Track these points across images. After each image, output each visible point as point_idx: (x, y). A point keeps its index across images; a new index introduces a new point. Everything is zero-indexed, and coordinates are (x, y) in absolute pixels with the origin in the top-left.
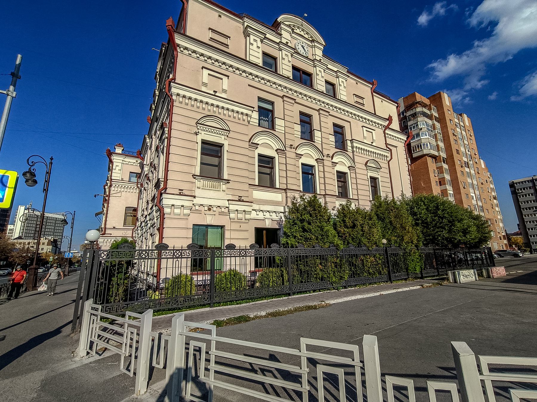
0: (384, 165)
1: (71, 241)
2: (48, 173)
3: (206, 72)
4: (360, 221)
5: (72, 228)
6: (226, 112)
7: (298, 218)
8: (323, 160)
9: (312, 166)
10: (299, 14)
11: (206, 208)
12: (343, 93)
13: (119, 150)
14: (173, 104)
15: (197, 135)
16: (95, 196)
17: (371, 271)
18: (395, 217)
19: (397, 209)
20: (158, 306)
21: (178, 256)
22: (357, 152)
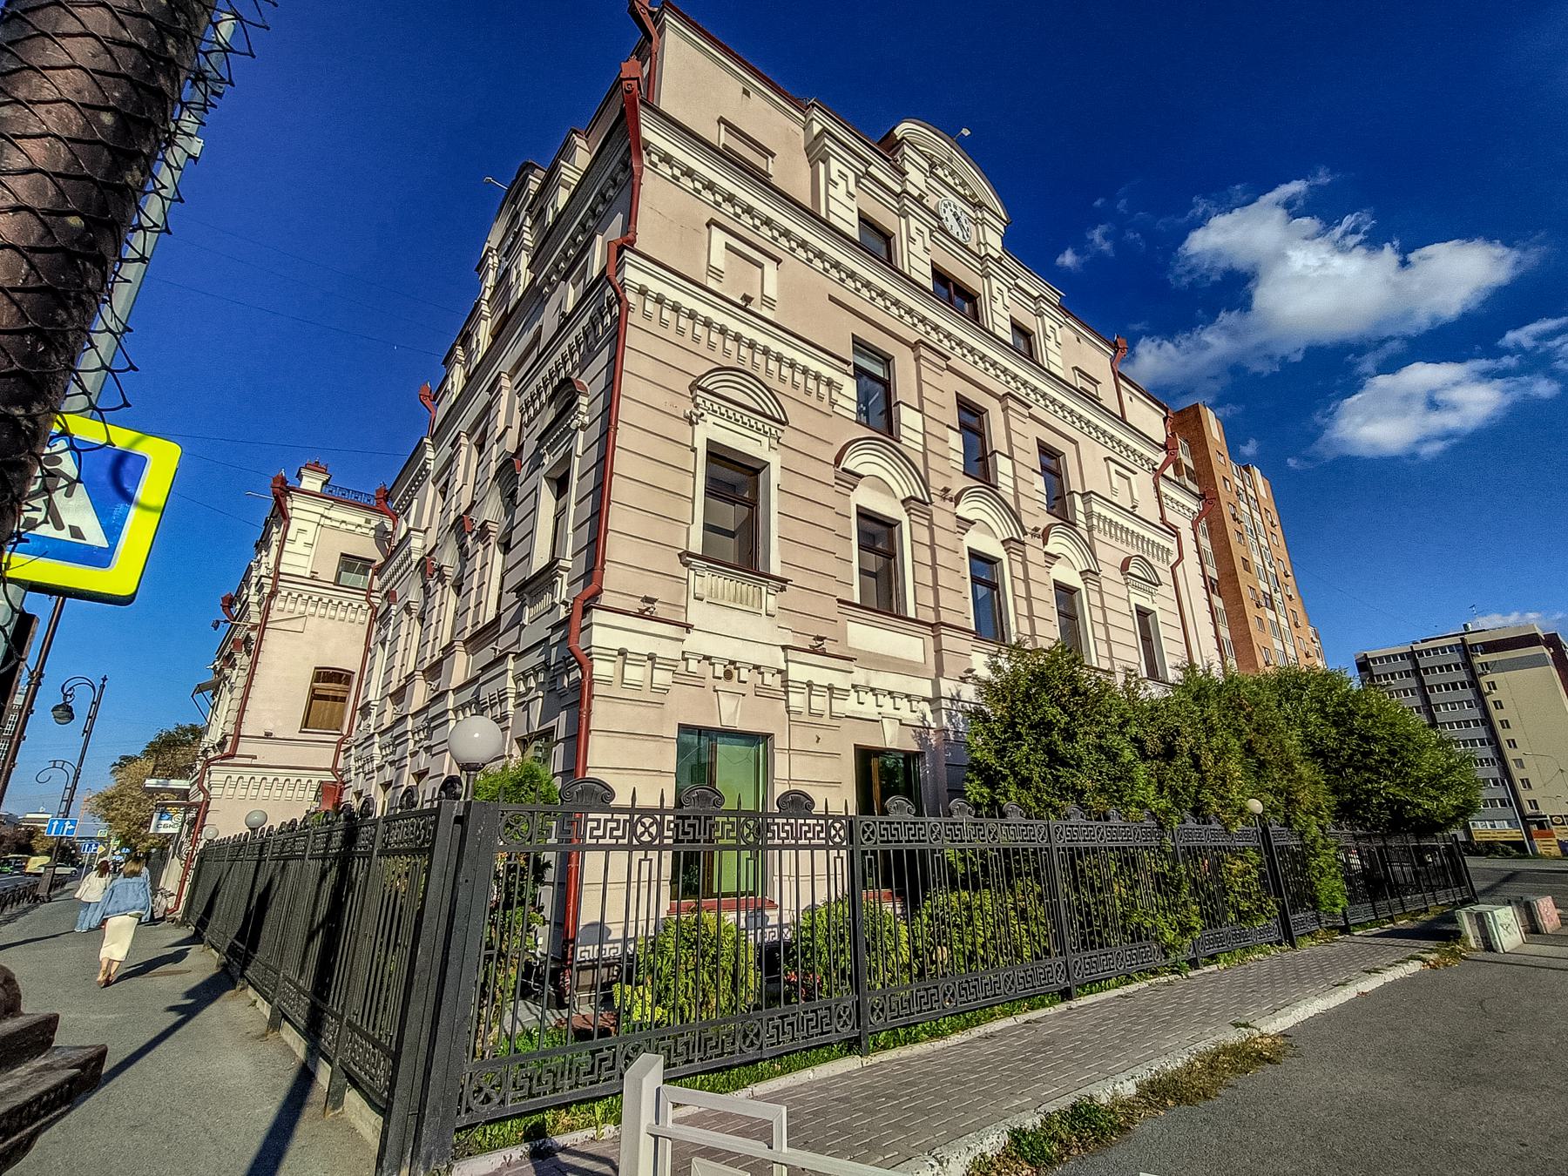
1: (77, 777)
5: (87, 733)
8: (1023, 543)
10: (947, 128)
11: (720, 671)
13: (312, 482)
20: (697, 1055)
21: (646, 838)
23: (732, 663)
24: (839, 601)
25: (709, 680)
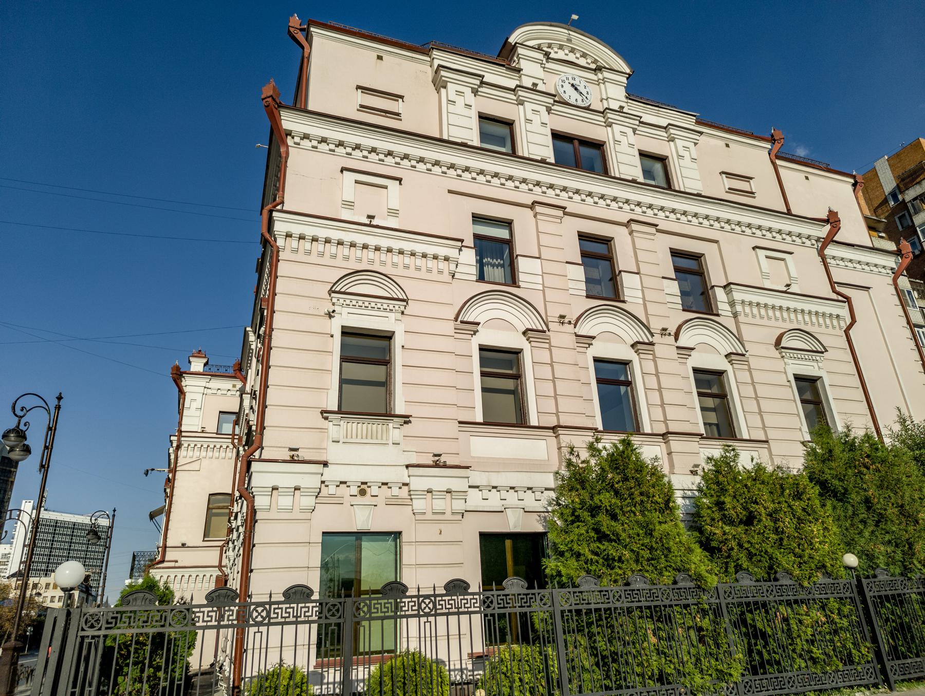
0: (833, 339)
2: (52, 429)
3: (350, 177)
4: (766, 504)
6: (396, 258)
7: (583, 503)
8: (652, 344)
9: (626, 363)
10: (558, 18)
11: (354, 490)
12: (687, 175)
13: (197, 365)
14: (278, 256)
15: (331, 317)
16: (147, 473)
17: (817, 652)
18: (881, 487)
19: (883, 461)
22: (746, 315)
23: (363, 483)
24: (460, 422)
25: (348, 500)
